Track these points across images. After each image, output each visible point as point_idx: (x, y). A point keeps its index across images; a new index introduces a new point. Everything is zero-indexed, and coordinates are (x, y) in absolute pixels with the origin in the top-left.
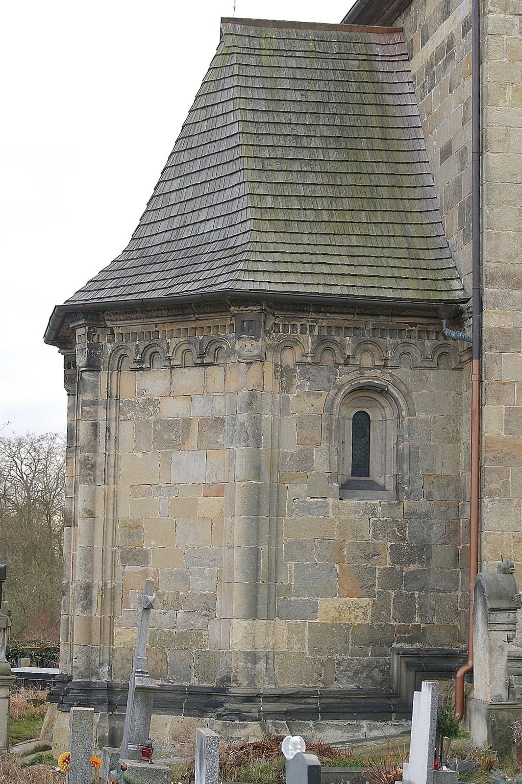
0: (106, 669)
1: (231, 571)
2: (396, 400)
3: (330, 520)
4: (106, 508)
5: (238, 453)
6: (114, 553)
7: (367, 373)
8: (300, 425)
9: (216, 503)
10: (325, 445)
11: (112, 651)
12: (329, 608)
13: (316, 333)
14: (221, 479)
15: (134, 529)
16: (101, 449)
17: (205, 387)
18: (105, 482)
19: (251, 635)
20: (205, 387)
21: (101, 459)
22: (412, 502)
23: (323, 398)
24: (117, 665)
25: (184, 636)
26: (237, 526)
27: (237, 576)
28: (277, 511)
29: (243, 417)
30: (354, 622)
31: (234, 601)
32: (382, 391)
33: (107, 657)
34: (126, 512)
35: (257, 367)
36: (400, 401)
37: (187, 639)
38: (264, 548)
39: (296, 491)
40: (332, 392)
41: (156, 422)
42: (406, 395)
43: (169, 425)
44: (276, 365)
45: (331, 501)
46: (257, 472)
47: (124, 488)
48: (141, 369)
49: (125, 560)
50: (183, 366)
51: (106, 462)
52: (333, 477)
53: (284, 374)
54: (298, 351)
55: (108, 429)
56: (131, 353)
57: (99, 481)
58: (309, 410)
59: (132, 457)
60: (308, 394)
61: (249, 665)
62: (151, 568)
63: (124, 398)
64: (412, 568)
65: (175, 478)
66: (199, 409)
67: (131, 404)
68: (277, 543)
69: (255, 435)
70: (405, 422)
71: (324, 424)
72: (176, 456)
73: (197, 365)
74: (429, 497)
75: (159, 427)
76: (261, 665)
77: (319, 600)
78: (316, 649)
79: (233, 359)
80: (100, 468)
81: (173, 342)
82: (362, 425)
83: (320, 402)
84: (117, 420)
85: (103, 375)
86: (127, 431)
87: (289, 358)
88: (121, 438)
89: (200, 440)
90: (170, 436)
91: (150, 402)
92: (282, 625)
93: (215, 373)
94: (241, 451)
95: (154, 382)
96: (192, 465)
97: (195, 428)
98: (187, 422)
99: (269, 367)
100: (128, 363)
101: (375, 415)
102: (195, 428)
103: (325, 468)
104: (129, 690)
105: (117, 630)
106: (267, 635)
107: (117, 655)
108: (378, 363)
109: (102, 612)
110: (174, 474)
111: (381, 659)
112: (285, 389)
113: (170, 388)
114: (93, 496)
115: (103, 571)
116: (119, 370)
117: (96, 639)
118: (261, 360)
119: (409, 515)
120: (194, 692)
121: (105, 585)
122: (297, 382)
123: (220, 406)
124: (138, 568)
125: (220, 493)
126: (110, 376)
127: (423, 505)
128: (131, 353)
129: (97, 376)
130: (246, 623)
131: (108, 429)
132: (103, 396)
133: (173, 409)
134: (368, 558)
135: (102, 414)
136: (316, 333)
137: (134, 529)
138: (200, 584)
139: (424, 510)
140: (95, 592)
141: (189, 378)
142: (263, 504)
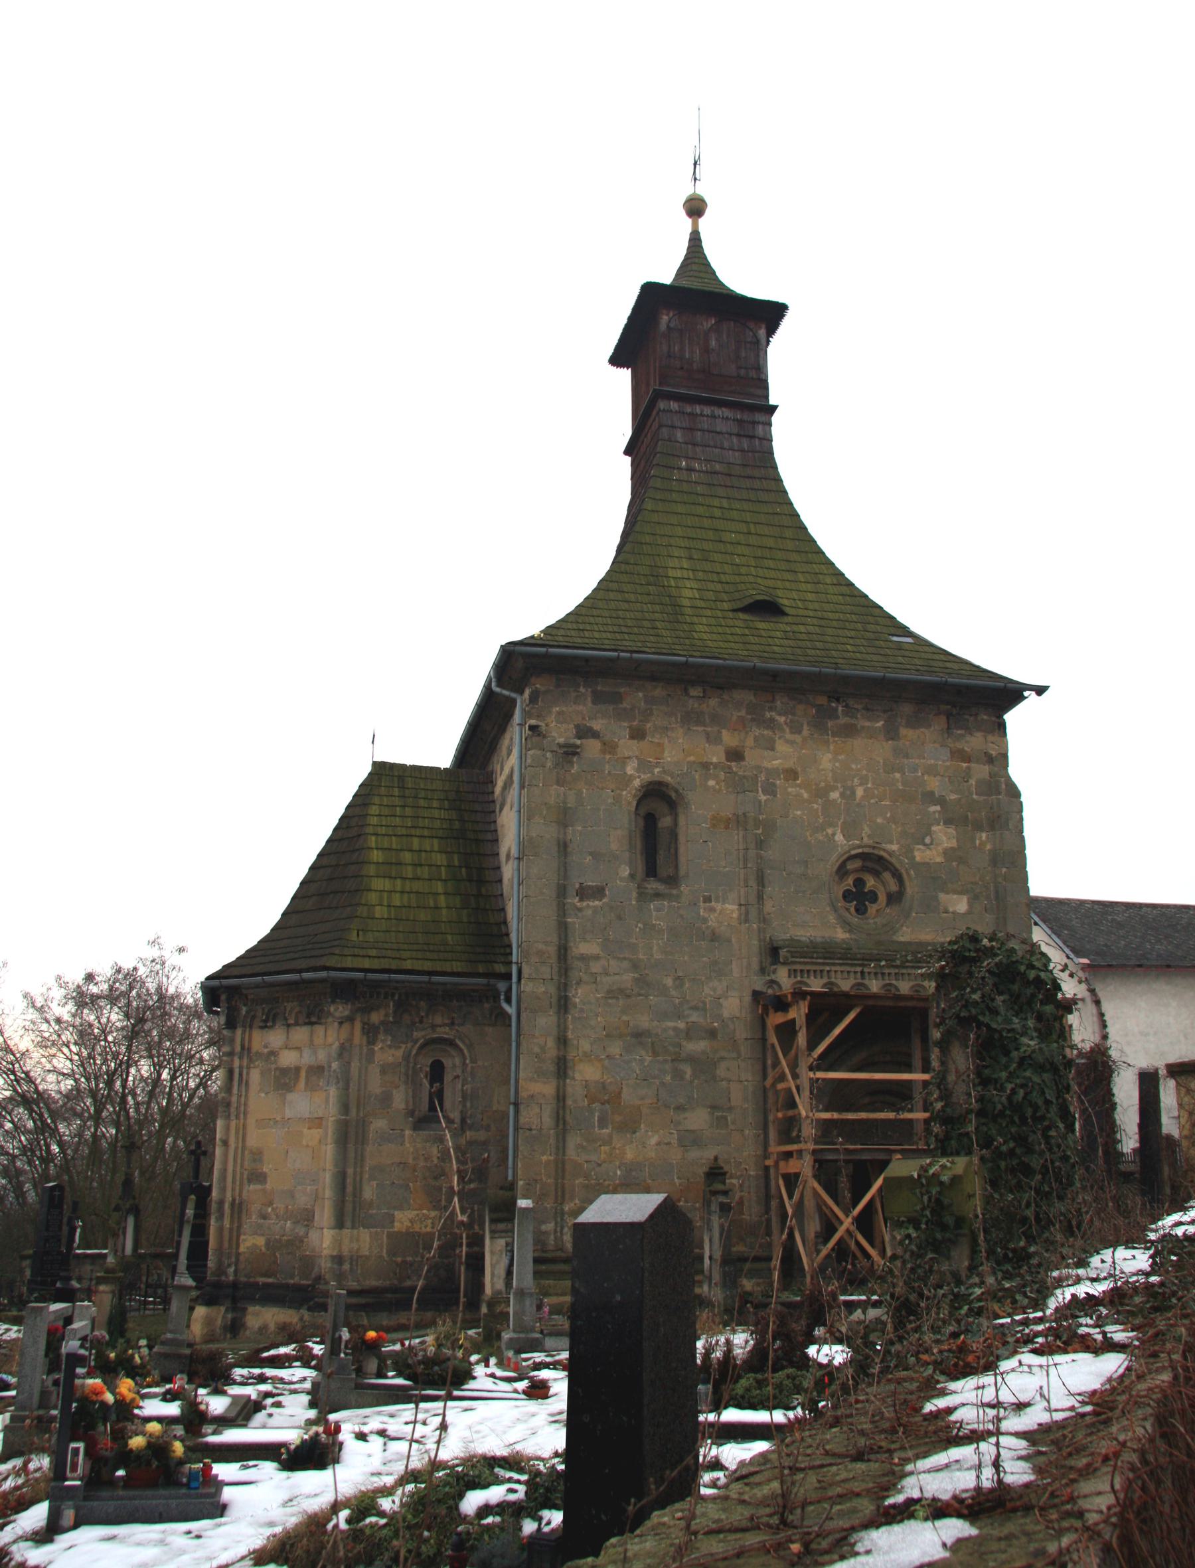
0: (232, 1269)
1: (324, 1189)
2: (461, 1050)
3: (396, 1147)
4: (237, 1138)
5: (332, 1093)
6: (242, 1174)
7: (438, 1029)
8: (383, 1072)
9: (316, 1133)
10: (402, 1088)
11: (238, 1255)
12: (403, 1220)
13: (396, 997)
14: (320, 1115)
15: (258, 1155)
16: (235, 1090)
17: (311, 1041)
18: (237, 1117)
19: (338, 1242)
20: (311, 1041)
21: (234, 1099)
22: (473, 1133)
23: (402, 1050)
24: (242, 1266)
25: (290, 1243)
26: (329, 1151)
27: (328, 1193)
28: (362, 1140)
29: (335, 1065)
30: (424, 1230)
31: (325, 1215)
32: (451, 1043)
33: (233, 1259)
34: (252, 1141)
35: (346, 1026)
36: (465, 1051)
37: (297, 1242)
38: (350, 1171)
39: (379, 1124)
40: (409, 1045)
41: (276, 1069)
42: (470, 1046)
43: (284, 1071)
44: (364, 1024)
45: (407, 1132)
46: (345, 1108)
47: (251, 1121)
48: (266, 1027)
49: (250, 1181)
50: (297, 1024)
51: (239, 1102)
52: (411, 1113)
53: (371, 1033)
54: (382, 1012)
55: (241, 1075)
56: (259, 1014)
57: (233, 1117)
58: (391, 1059)
59: (259, 1100)
60: (390, 1047)
61: (335, 1266)
62: (268, 1186)
63: (254, 1050)
64: (472, 1186)
65: (288, 1113)
66: (307, 1059)
67: (259, 1055)
68: (362, 1167)
69: (345, 1081)
70: (469, 1069)
71: (403, 1070)
72: (290, 1096)
73: (306, 1024)
74: (488, 1128)
75: (278, 1073)
76: (346, 1266)
77: (396, 1213)
78: (392, 1252)
79: (330, 1019)
80: (234, 1105)
81: (289, 1006)
82: (437, 1072)
83: (399, 1053)
84: (248, 1068)
85: (239, 1032)
86: (255, 1076)
87: (375, 1018)
88: (251, 1082)
89: (307, 1084)
90: (285, 1080)
91: (273, 1053)
92: (365, 1235)
93: (319, 1030)
94: (333, 1092)
95: (275, 1038)
96: (301, 1103)
97: (303, 1074)
98: (298, 1069)
99: (358, 1026)
100: (257, 1023)
101: (447, 1063)
102: (303, 1074)
103: (403, 1106)
104: (530, 1267)
105: (242, 1237)
106: (351, 1241)
107: (242, 1258)
108: (447, 1021)
109: (232, 1222)
110: (287, 1111)
111: (446, 1261)
112: (371, 1042)
113: (291, 1045)
114: (227, 1128)
115: (233, 1189)
116: (251, 1027)
117: (226, 1245)
118: (350, 1019)
119: (470, 1143)
120: (298, 1288)
121: (234, 1200)
122: (381, 1037)
123: (322, 1056)
124: (259, 1187)
125: (319, 1126)
126: (244, 1033)
127: (481, 1136)
128: (259, 1014)
129: (234, 1033)
130: (332, 1232)
131: (241, 1075)
132: (238, 1049)
133: (288, 1059)
134: (436, 1178)
135: (237, 1063)
136: (396, 997)
137: (258, 1155)
138: (302, 1200)
139: (483, 1139)
140: (227, 1206)
141: (300, 1034)
142: (350, 1135)
